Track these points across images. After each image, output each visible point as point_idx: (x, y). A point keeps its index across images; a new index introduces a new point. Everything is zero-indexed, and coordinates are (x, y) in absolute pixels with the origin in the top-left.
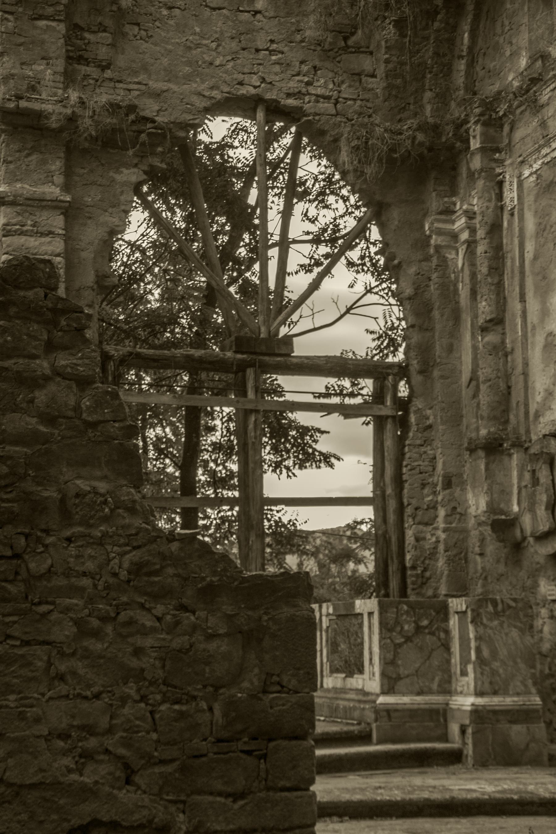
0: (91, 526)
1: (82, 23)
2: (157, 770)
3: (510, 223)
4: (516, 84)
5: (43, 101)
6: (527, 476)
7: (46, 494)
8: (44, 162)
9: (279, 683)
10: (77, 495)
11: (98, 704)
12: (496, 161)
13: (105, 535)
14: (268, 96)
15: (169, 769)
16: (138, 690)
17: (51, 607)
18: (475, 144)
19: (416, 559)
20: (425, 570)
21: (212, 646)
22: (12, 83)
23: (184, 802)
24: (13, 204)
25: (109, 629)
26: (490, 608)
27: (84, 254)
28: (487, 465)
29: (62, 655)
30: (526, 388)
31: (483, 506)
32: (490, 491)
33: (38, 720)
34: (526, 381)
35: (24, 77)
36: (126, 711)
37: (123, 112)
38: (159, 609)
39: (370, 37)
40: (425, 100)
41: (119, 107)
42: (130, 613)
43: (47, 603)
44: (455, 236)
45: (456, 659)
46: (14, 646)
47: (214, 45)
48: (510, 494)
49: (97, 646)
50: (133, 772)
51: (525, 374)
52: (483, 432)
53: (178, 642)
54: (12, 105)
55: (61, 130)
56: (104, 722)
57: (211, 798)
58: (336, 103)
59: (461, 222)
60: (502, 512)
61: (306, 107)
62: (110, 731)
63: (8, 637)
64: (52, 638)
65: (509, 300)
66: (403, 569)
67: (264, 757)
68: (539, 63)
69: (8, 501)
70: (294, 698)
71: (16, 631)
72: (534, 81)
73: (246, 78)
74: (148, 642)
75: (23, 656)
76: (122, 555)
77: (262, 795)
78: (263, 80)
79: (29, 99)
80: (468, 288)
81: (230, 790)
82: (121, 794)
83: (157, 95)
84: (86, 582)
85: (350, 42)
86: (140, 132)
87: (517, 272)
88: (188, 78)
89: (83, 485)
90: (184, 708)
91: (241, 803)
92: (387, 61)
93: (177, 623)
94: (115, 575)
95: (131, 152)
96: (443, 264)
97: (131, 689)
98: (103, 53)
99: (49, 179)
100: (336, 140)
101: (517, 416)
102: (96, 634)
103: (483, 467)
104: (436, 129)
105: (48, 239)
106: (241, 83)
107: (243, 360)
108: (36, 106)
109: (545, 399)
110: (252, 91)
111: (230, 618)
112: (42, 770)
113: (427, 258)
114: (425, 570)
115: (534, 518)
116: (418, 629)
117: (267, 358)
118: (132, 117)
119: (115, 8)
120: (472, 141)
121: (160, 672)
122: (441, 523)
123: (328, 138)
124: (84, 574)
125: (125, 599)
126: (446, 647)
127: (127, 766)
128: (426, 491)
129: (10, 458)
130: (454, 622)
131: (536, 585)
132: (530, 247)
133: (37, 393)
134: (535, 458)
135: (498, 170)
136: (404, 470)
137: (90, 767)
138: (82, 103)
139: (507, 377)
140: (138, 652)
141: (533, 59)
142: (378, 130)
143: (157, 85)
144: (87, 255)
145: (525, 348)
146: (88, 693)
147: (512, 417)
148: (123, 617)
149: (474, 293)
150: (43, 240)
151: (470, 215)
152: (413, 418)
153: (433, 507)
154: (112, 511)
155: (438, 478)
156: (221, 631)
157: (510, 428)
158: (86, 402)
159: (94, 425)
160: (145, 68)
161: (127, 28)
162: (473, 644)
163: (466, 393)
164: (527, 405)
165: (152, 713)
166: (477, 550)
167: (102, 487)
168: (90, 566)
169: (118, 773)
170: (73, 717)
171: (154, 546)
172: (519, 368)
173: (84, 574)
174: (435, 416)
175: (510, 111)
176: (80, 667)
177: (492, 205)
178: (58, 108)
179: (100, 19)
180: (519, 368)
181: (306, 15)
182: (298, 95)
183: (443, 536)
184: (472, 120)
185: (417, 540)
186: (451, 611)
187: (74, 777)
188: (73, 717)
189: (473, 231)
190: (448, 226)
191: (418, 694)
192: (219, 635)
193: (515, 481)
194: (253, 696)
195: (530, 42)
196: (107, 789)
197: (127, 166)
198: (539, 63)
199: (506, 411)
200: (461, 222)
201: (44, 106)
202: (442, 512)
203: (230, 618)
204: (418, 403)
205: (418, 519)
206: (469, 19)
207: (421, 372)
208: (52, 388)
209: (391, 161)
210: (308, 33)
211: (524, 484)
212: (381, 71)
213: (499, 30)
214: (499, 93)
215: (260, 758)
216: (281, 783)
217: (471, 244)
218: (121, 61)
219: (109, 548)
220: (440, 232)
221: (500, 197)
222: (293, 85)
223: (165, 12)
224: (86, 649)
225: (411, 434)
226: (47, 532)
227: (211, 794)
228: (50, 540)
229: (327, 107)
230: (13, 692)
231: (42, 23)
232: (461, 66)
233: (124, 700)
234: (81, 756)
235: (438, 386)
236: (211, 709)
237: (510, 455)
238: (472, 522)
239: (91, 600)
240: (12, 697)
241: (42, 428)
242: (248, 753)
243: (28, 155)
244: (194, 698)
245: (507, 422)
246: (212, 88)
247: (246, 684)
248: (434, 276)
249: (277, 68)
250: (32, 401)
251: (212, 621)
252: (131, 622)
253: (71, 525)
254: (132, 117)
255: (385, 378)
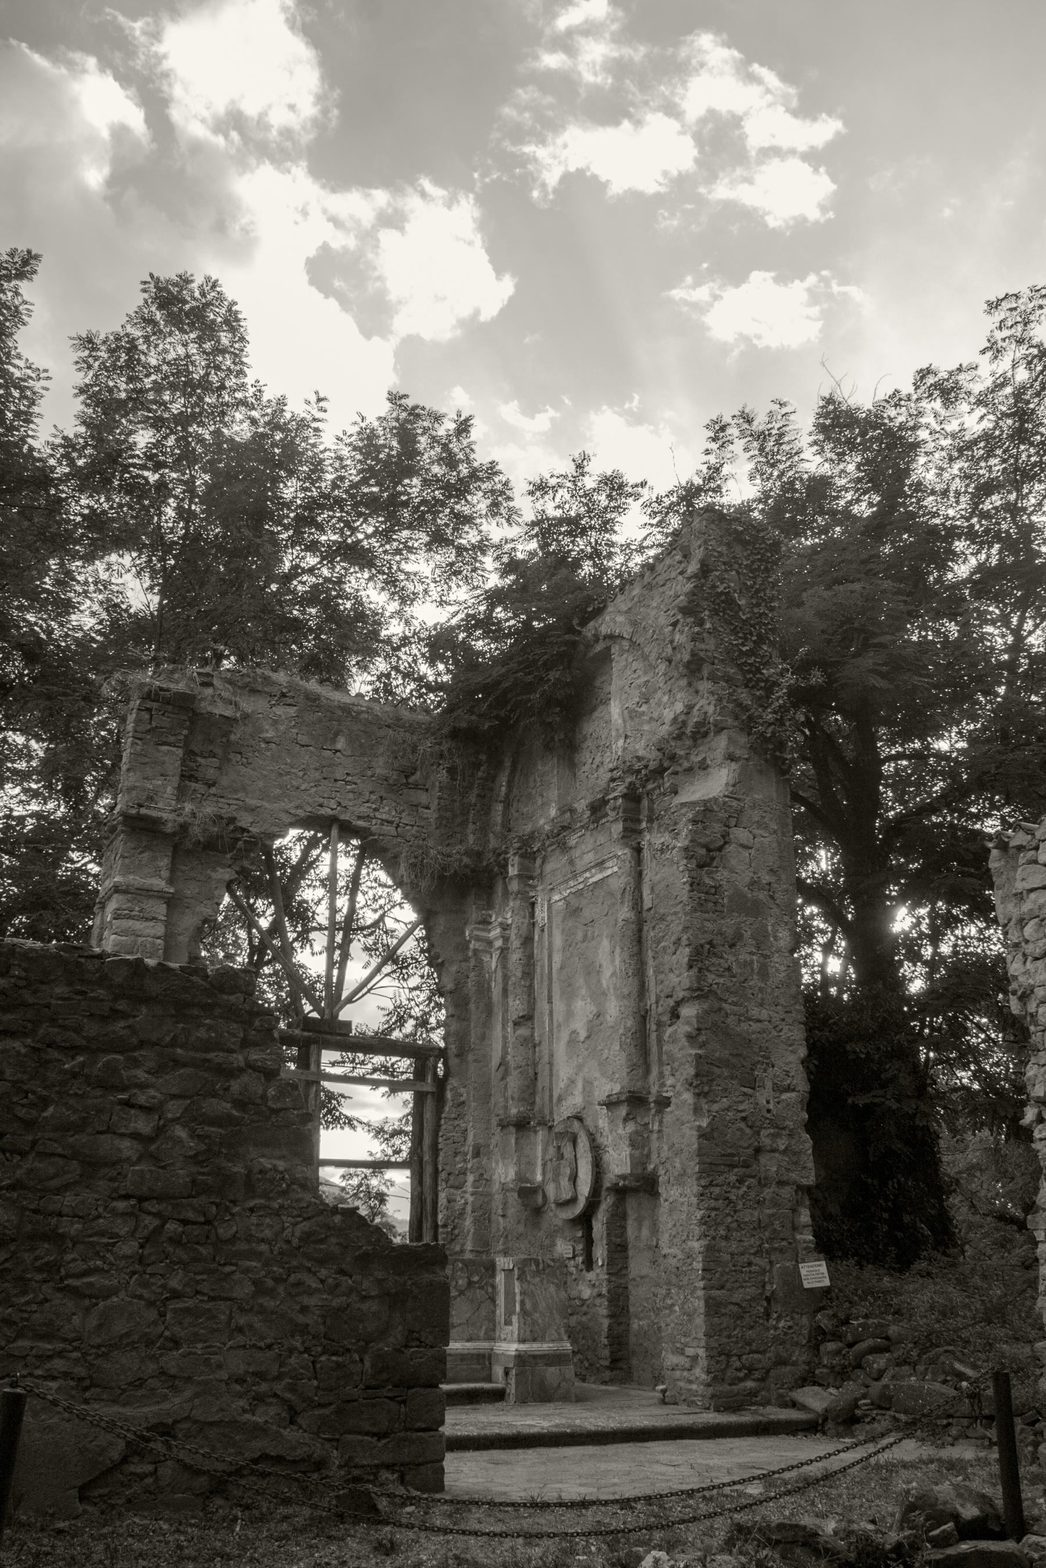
0: (269, 1199)
1: (196, 750)
2: (316, 1412)
3: (541, 937)
4: (547, 828)
5: (160, 810)
6: (552, 1151)
7: (235, 1170)
8: (154, 859)
9: (418, 1339)
10: (261, 1172)
11: (270, 1354)
12: (530, 886)
13: (282, 1207)
14: (342, 817)
15: (326, 1411)
16: (303, 1342)
17: (233, 1268)
18: (512, 871)
19: (448, 1218)
20: (454, 1228)
21: (365, 1306)
22: (134, 793)
23: (338, 1440)
24: (126, 892)
25: (281, 1289)
26: (534, 1267)
27: (180, 938)
28: (517, 1139)
29: (242, 1310)
30: (551, 1075)
31: (512, 1174)
32: (518, 1163)
33: (220, 1366)
34: (551, 1070)
35: (144, 790)
36: (293, 1360)
37: (224, 822)
38: (323, 1273)
39: (427, 778)
40: (469, 831)
41: (222, 818)
42: (299, 1276)
43: (231, 1264)
44: (490, 943)
45: (501, 1311)
46: (202, 1301)
47: (301, 774)
48: (534, 1165)
49: (270, 1303)
50: (296, 1413)
51: (551, 1064)
52: (514, 1111)
53: (336, 1302)
54: (134, 811)
55: (174, 834)
56: (274, 1370)
57: (360, 1437)
58: (398, 826)
59: (496, 932)
60: (528, 1181)
61: (374, 828)
62: (279, 1378)
63: (198, 1292)
64: (234, 1295)
65: (538, 1001)
66: (436, 1227)
67: (404, 1402)
68: (568, 815)
69: (203, 1174)
70: (430, 1352)
71: (205, 1288)
72: (564, 828)
73: (326, 802)
74: (312, 1301)
75: (209, 1310)
76: (295, 1224)
77: (402, 1434)
78: (339, 804)
79: (148, 808)
80: (500, 987)
81: (375, 1430)
82: (286, 1433)
83: (252, 810)
84: (263, 1247)
85: (411, 780)
86: (238, 839)
87: (545, 978)
88: (277, 799)
89: (267, 1163)
90: (340, 1359)
91: (384, 1441)
92: (440, 798)
93: (337, 1285)
94: (288, 1242)
95: (228, 856)
96: (480, 965)
97: (297, 1343)
98: (211, 773)
99: (157, 873)
100: (396, 857)
101: (542, 1098)
102: (271, 1293)
103: (513, 1141)
104: (479, 855)
105: (151, 924)
106: (321, 805)
107: (309, 1037)
108: (154, 814)
109: (568, 1086)
110: (330, 812)
111: (380, 1282)
112: (222, 1410)
113: (466, 960)
114: (454, 1228)
115: (558, 1187)
116: (470, 1284)
117: (329, 1037)
118: (231, 827)
119: (224, 740)
120: (510, 869)
121: (322, 1327)
122: (469, 1187)
123: (390, 855)
124: (263, 1240)
125: (295, 1263)
126: (493, 1300)
127: (291, 1408)
128: (458, 1159)
129: (208, 1137)
130: (500, 1279)
131: (553, 1244)
132: (557, 959)
133: (232, 1083)
134: (560, 1136)
135: (532, 894)
136: (440, 1140)
137: (261, 1409)
138: (194, 815)
139: (535, 1065)
140: (304, 1309)
141: (562, 811)
142: (433, 852)
143: (252, 802)
144: (183, 939)
145: (551, 1043)
146: (262, 1344)
147: (538, 1099)
148: (292, 1279)
149: (505, 992)
150: (147, 924)
151: (505, 927)
152: (449, 1095)
153: (463, 1173)
154: (288, 1186)
155: (469, 1148)
156: (373, 1293)
157: (536, 1108)
158: (271, 1092)
159: (277, 1112)
160: (244, 788)
161: (232, 756)
162: (518, 1298)
163: (495, 1076)
164: (551, 1090)
165: (313, 1362)
166: (500, 1212)
167: (281, 1165)
168: (268, 1233)
169: (284, 1415)
170: (249, 1364)
171: (321, 1218)
172: (546, 1059)
173: (263, 1240)
174: (468, 1094)
175: (543, 848)
176: (256, 1321)
177: (526, 921)
178: (171, 816)
179: (211, 748)
180: (546, 1059)
181: (376, 756)
182: (367, 818)
183: (471, 1199)
184: (512, 852)
185: (449, 1201)
186: (498, 1268)
187: (248, 1416)
188: (249, 1364)
189: (506, 939)
190: (484, 934)
191: (468, 1341)
192: (370, 1297)
193: (539, 1154)
194: (399, 1351)
195: (559, 795)
196: (274, 1427)
197: (224, 866)
198: (568, 815)
199: (533, 1094)
200: (496, 932)
201: (160, 814)
202: (471, 1178)
203: (380, 1282)
204: (453, 1082)
205: (450, 1183)
206: (507, 772)
207: (457, 1056)
208: (245, 1078)
209: (441, 878)
210: (378, 771)
211: (548, 1157)
212: (434, 805)
213: (532, 784)
214: (533, 832)
215: (400, 1403)
216: (418, 1425)
217: (504, 951)
218: (224, 781)
219: (284, 1218)
220: (478, 939)
221: (532, 915)
222: (364, 809)
223: (263, 745)
224: (261, 1306)
225: (447, 1109)
226: (234, 1202)
227: (360, 1433)
228: (235, 1210)
229: (390, 829)
230: (201, 1341)
231: (165, 748)
232: (500, 807)
233: (291, 1351)
234: (254, 1399)
235: (472, 1067)
236: (362, 1360)
237: (536, 1132)
238: (496, 1187)
239: (267, 1264)
240: (200, 1345)
241: (235, 1113)
242: (391, 1399)
243: (142, 852)
244: (348, 1350)
245: (534, 1103)
246: (297, 807)
247: (391, 1339)
248: (472, 975)
249: (351, 796)
250: (227, 1089)
251: (366, 1284)
252: (299, 1284)
253: (253, 1198)
254: (231, 827)
255: (427, 1059)
